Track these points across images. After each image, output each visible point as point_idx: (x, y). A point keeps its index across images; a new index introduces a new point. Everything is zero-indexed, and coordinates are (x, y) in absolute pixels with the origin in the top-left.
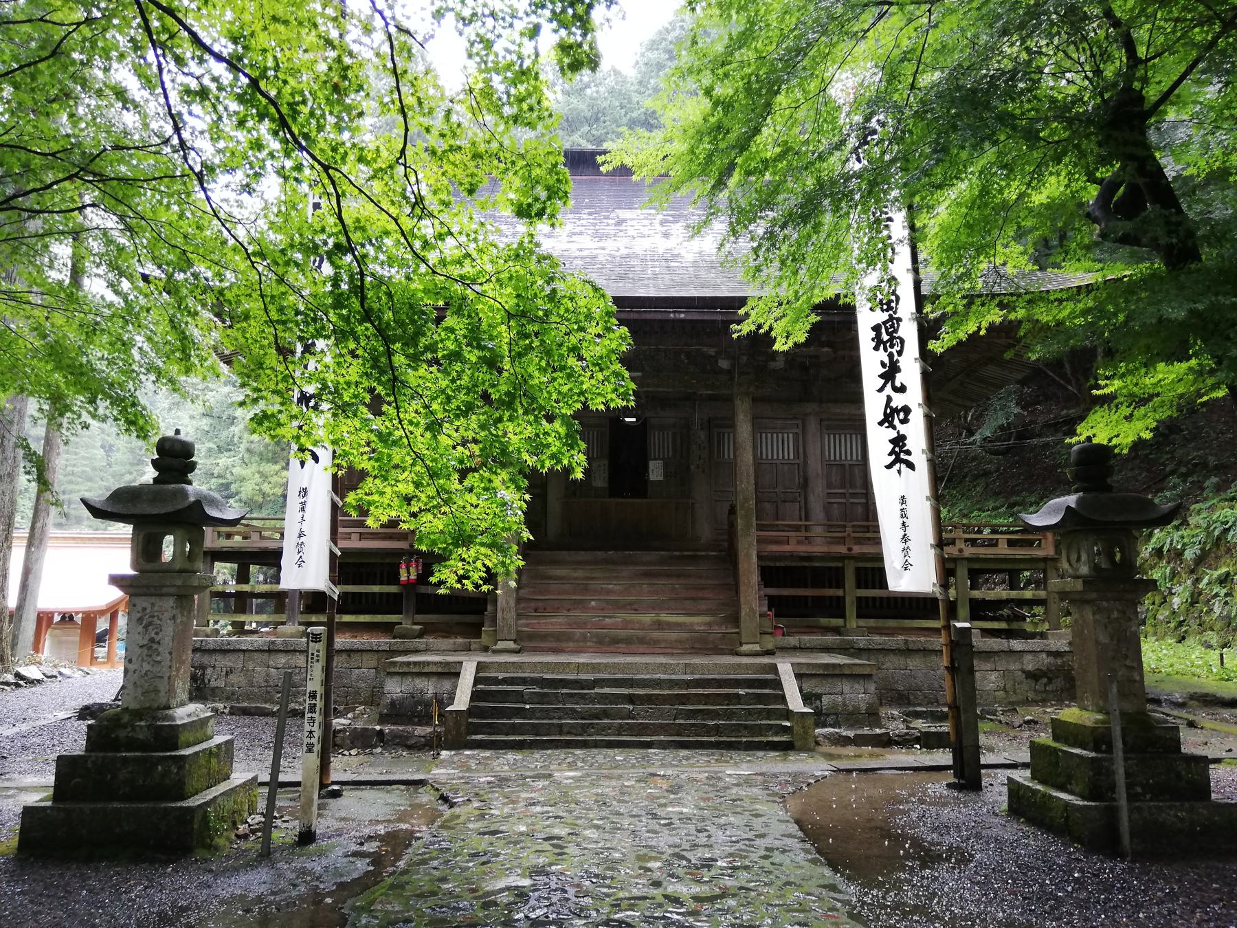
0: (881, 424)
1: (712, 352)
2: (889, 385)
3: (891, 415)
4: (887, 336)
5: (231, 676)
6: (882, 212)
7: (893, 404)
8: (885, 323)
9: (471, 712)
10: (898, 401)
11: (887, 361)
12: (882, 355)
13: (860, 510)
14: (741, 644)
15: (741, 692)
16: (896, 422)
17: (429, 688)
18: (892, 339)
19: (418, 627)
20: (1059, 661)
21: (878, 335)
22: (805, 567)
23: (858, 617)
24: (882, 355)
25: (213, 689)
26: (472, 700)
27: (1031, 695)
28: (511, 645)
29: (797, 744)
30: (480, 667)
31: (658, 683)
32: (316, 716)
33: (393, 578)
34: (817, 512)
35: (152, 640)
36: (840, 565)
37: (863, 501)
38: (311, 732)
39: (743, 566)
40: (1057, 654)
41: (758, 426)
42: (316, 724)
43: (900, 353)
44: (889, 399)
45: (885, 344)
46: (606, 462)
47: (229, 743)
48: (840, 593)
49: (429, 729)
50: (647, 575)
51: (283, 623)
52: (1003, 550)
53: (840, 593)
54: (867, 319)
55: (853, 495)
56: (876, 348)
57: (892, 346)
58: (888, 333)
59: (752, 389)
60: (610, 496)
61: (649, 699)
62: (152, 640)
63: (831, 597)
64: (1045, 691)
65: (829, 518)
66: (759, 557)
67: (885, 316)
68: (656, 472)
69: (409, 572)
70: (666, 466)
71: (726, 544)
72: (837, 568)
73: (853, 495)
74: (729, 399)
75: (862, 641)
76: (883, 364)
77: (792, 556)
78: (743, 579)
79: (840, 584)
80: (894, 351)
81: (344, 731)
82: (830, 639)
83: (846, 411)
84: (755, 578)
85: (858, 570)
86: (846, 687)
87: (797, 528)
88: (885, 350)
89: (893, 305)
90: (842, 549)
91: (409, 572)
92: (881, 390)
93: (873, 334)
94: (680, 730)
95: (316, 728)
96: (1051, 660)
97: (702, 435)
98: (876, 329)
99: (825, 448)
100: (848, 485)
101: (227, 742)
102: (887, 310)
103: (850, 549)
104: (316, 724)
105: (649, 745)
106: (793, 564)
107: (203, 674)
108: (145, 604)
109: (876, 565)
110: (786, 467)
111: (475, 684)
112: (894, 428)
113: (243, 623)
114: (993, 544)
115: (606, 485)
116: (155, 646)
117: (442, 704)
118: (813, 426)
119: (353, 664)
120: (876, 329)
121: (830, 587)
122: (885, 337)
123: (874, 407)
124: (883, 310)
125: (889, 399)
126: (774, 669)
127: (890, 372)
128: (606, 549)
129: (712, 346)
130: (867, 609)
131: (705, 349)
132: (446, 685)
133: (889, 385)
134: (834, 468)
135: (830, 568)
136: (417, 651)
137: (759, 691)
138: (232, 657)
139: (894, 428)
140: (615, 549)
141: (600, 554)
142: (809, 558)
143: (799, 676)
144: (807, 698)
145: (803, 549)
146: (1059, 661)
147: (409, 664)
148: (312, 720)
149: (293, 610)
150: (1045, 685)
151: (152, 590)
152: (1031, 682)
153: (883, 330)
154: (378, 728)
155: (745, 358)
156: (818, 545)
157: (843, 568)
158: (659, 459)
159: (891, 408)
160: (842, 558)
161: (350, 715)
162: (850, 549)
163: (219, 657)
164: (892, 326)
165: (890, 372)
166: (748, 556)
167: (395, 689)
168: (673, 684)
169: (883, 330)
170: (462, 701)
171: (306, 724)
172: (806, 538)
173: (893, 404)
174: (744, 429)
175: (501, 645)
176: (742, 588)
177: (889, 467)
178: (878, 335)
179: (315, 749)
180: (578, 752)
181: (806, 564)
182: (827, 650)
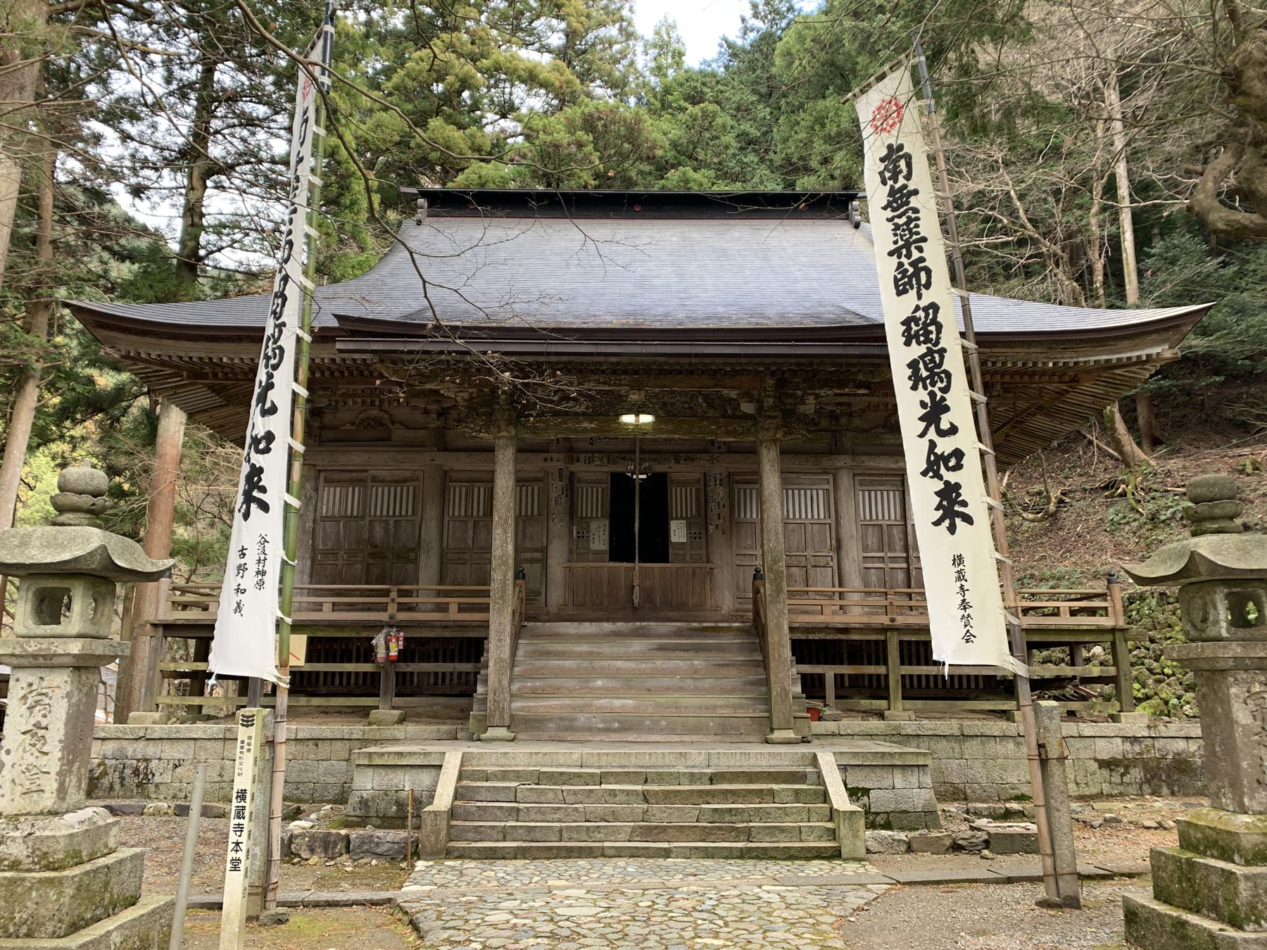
0: (924, 474)
1: (733, 394)
2: (932, 429)
3: (936, 462)
4: (929, 371)
5: (178, 770)
6: (911, 234)
7: (938, 451)
8: (922, 357)
9: (452, 813)
10: (945, 446)
11: (927, 400)
12: (922, 395)
13: (901, 576)
14: (772, 730)
15: (775, 787)
16: (943, 471)
17: (407, 783)
18: (931, 377)
19: (398, 712)
20: (1137, 749)
21: (909, 329)
22: (841, 641)
23: (904, 698)
24: (922, 395)
25: (157, 786)
26: (455, 798)
27: (1106, 788)
28: (502, 732)
29: (845, 852)
30: (465, 759)
31: (677, 778)
32: (245, 822)
33: (367, 653)
34: (854, 580)
35: (38, 726)
36: (882, 638)
37: (905, 565)
38: (237, 844)
39: (772, 638)
40: (1135, 740)
41: (786, 483)
42: (245, 834)
43: (945, 390)
44: (932, 445)
45: (924, 380)
46: (607, 523)
47: (138, 858)
48: (881, 670)
49: (402, 834)
50: (663, 648)
51: (377, 708)
52: (1065, 620)
53: (881, 670)
54: (900, 355)
55: (893, 559)
56: (914, 388)
57: (933, 384)
58: (927, 369)
59: (779, 435)
60: (612, 559)
61: (668, 796)
62: (38, 726)
63: (870, 676)
64: (1122, 783)
65: (866, 584)
66: (791, 629)
67: (923, 349)
68: (678, 533)
69: (388, 648)
70: (689, 526)
71: (750, 615)
72: (877, 642)
73: (893, 559)
74: (753, 451)
75: (910, 727)
76: (923, 404)
77: (826, 628)
78: (773, 653)
79: (882, 659)
80: (936, 389)
81: (302, 835)
82: (874, 724)
83: (882, 465)
84: (787, 653)
85: (901, 643)
86: (899, 779)
87: (830, 596)
88: (925, 388)
89: (933, 336)
90: (884, 620)
91: (388, 648)
92: (922, 435)
93: (909, 372)
94: (705, 834)
95: (244, 838)
96: (1128, 746)
97: (721, 492)
98: (913, 365)
99: (862, 507)
100: (886, 548)
101: (134, 857)
102: (925, 342)
103: (893, 620)
104: (245, 834)
105: (666, 853)
106: (829, 637)
107: (146, 768)
108: (30, 679)
109: (923, 638)
110: (816, 527)
111: (460, 778)
112: (940, 478)
113: (200, 707)
114: (1056, 613)
115: (605, 547)
116: (41, 732)
117: (419, 803)
118: (845, 480)
119: (322, 755)
120: (913, 365)
121: (870, 664)
122: (924, 373)
123: (915, 454)
124: (919, 343)
125: (932, 445)
126: (814, 760)
127: (934, 412)
128: (614, 620)
129: (733, 388)
130: (918, 690)
131: (725, 392)
132: (425, 778)
133: (932, 429)
134: (870, 529)
135: (869, 642)
136: (396, 740)
137: (797, 786)
138: (182, 746)
139: (940, 478)
140: (626, 620)
141: (607, 626)
142: (846, 630)
143: (844, 768)
144: (854, 793)
145: (839, 620)
146: (1137, 749)
147: (401, 754)
148: (239, 828)
149: (255, 693)
150: (1122, 775)
151: (41, 660)
152: (1106, 773)
153: (921, 366)
154: (343, 832)
155: (771, 400)
156: (857, 613)
157: (885, 642)
158: (682, 518)
159: (936, 455)
160: (884, 630)
161: (313, 816)
162: (893, 620)
163: (166, 746)
164: (933, 360)
165: (934, 412)
166: (779, 626)
167: (367, 784)
168: (693, 778)
169: (921, 366)
170: (443, 800)
171: (232, 834)
172: (841, 607)
173: (938, 451)
174: (771, 481)
175: (492, 732)
176: (772, 665)
177: (937, 523)
178: (909, 329)
179: (242, 866)
180: (582, 862)
181: (843, 637)
182: (871, 736)
